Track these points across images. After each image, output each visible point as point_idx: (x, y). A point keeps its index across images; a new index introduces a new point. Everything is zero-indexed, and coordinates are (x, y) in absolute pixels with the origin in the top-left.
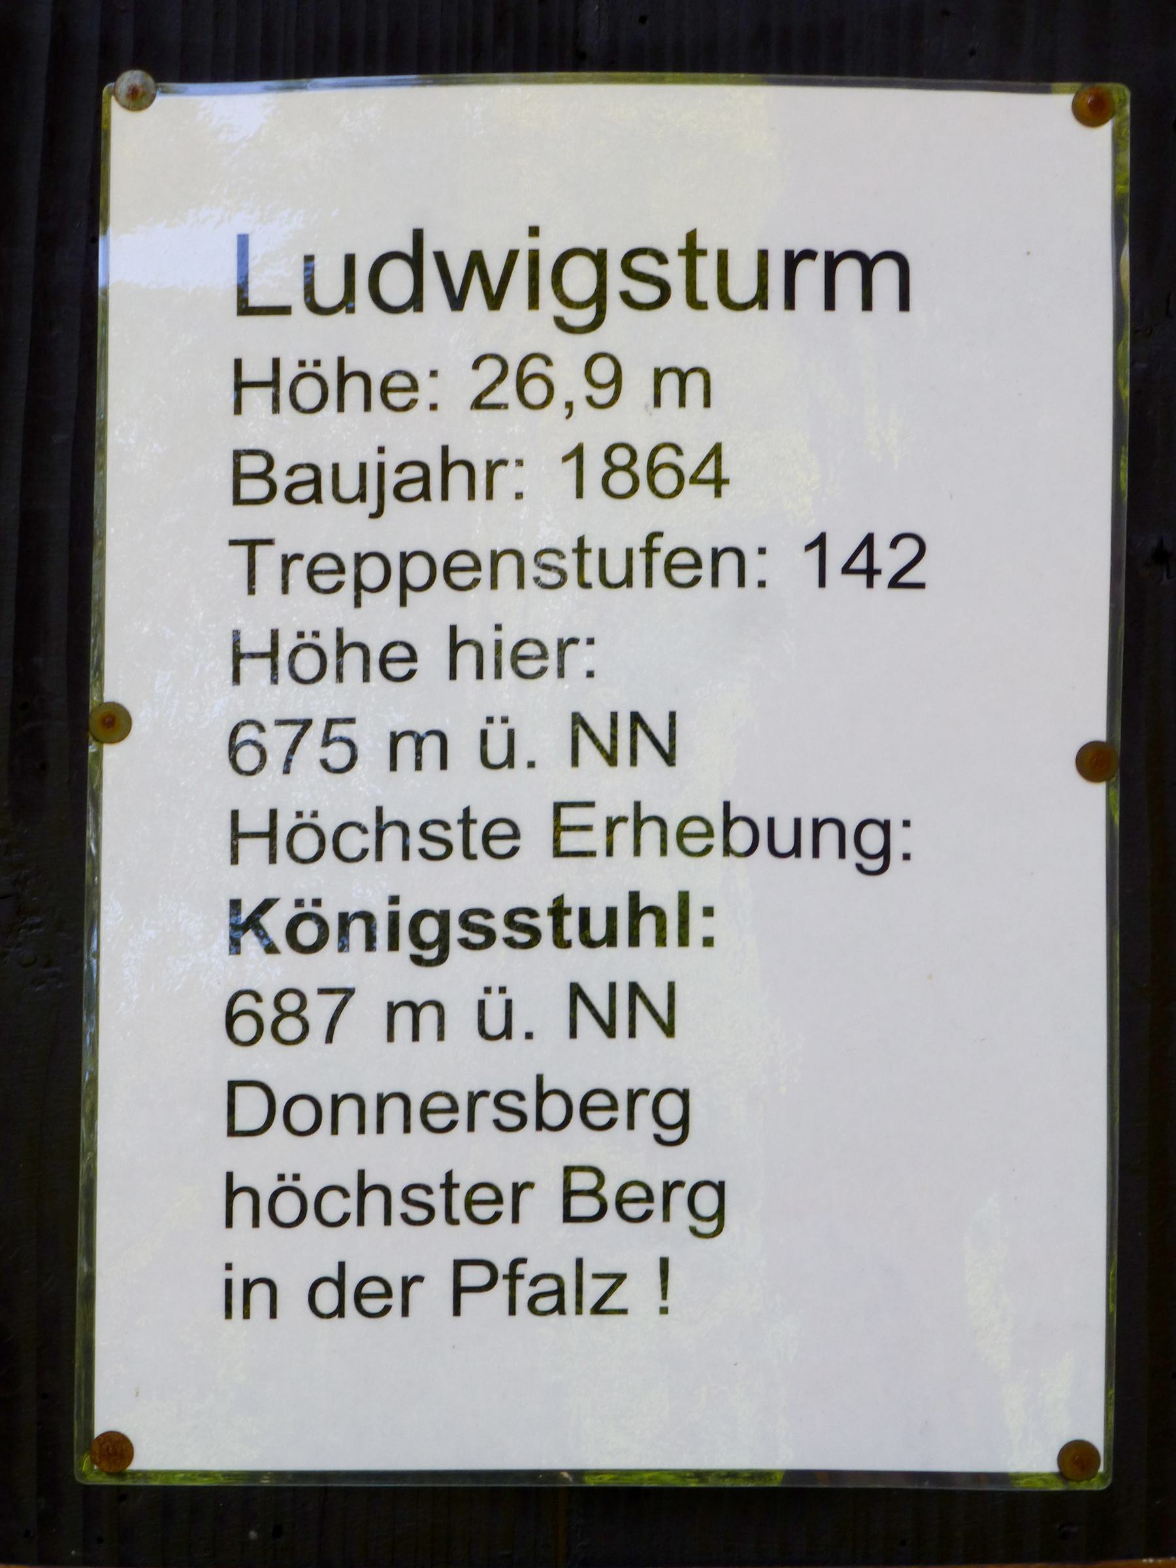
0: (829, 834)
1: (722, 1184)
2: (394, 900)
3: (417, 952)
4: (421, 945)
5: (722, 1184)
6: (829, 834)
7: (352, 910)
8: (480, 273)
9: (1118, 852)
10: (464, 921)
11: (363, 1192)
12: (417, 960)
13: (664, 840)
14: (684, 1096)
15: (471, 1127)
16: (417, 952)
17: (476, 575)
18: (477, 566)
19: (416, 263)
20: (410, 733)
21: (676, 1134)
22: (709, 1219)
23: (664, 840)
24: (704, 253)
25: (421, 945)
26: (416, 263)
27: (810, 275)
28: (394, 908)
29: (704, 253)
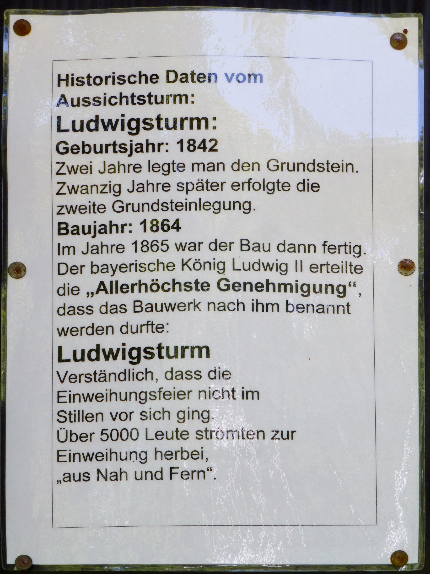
0: (237, 205)
1: (250, 202)
2: (105, 94)
3: (303, 293)
4: (339, 293)
5: (250, 202)
6: (237, 205)
7: (194, 117)
8: (111, 126)
9: (287, 10)
10: (145, 351)
11: (238, 304)
12: (303, 295)
13: (240, 207)
14: (224, 263)
15: (80, 382)
16: (303, 293)
17: (218, 187)
18: (218, 186)
19: (259, 264)
20: (251, 391)
21: (248, 211)
22: (222, 270)
23: (240, 207)
24: (208, 431)
25: (339, 293)
26: (259, 264)
27: (195, 474)
28: (131, 143)
29: (208, 431)
